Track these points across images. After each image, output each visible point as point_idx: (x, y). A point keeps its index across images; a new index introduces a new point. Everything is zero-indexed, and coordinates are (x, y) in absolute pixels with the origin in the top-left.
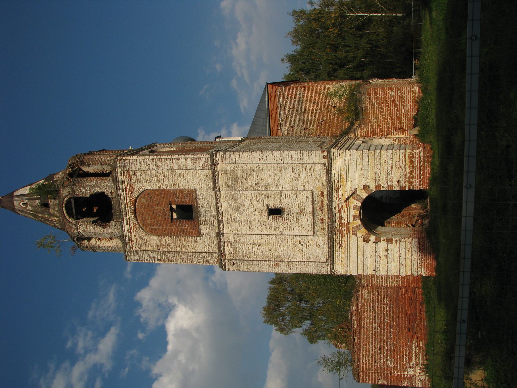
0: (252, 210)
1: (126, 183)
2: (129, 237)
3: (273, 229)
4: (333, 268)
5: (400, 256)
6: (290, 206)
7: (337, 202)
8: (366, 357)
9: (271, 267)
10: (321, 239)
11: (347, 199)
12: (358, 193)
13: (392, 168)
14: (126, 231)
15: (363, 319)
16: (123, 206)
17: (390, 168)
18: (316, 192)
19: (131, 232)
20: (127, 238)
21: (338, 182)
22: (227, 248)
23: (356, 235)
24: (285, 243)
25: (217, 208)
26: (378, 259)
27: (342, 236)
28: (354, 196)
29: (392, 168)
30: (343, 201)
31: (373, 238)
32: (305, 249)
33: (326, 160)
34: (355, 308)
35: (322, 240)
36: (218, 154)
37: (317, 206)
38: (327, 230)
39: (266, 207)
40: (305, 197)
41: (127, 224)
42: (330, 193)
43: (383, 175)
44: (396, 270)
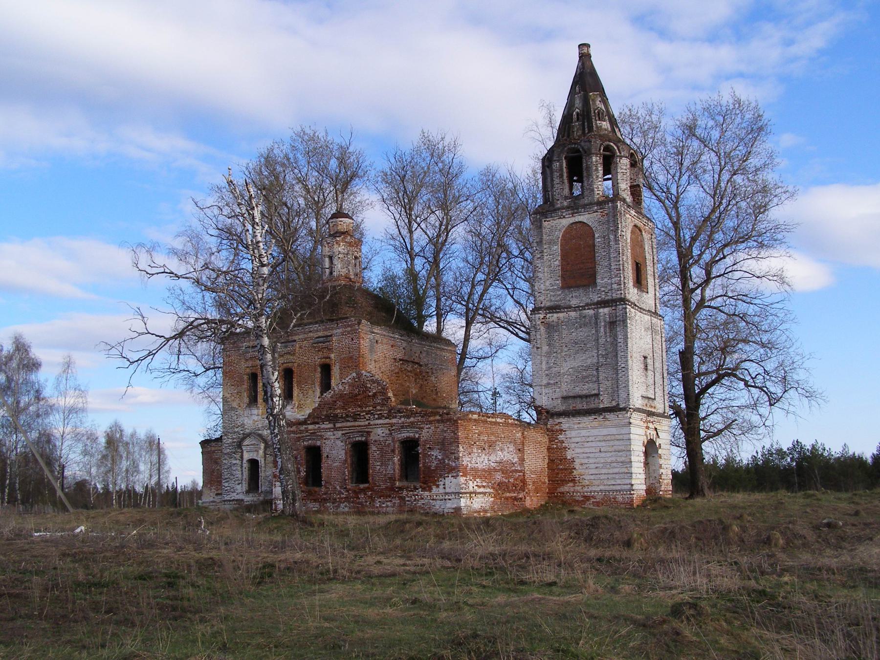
4: (634, 411)
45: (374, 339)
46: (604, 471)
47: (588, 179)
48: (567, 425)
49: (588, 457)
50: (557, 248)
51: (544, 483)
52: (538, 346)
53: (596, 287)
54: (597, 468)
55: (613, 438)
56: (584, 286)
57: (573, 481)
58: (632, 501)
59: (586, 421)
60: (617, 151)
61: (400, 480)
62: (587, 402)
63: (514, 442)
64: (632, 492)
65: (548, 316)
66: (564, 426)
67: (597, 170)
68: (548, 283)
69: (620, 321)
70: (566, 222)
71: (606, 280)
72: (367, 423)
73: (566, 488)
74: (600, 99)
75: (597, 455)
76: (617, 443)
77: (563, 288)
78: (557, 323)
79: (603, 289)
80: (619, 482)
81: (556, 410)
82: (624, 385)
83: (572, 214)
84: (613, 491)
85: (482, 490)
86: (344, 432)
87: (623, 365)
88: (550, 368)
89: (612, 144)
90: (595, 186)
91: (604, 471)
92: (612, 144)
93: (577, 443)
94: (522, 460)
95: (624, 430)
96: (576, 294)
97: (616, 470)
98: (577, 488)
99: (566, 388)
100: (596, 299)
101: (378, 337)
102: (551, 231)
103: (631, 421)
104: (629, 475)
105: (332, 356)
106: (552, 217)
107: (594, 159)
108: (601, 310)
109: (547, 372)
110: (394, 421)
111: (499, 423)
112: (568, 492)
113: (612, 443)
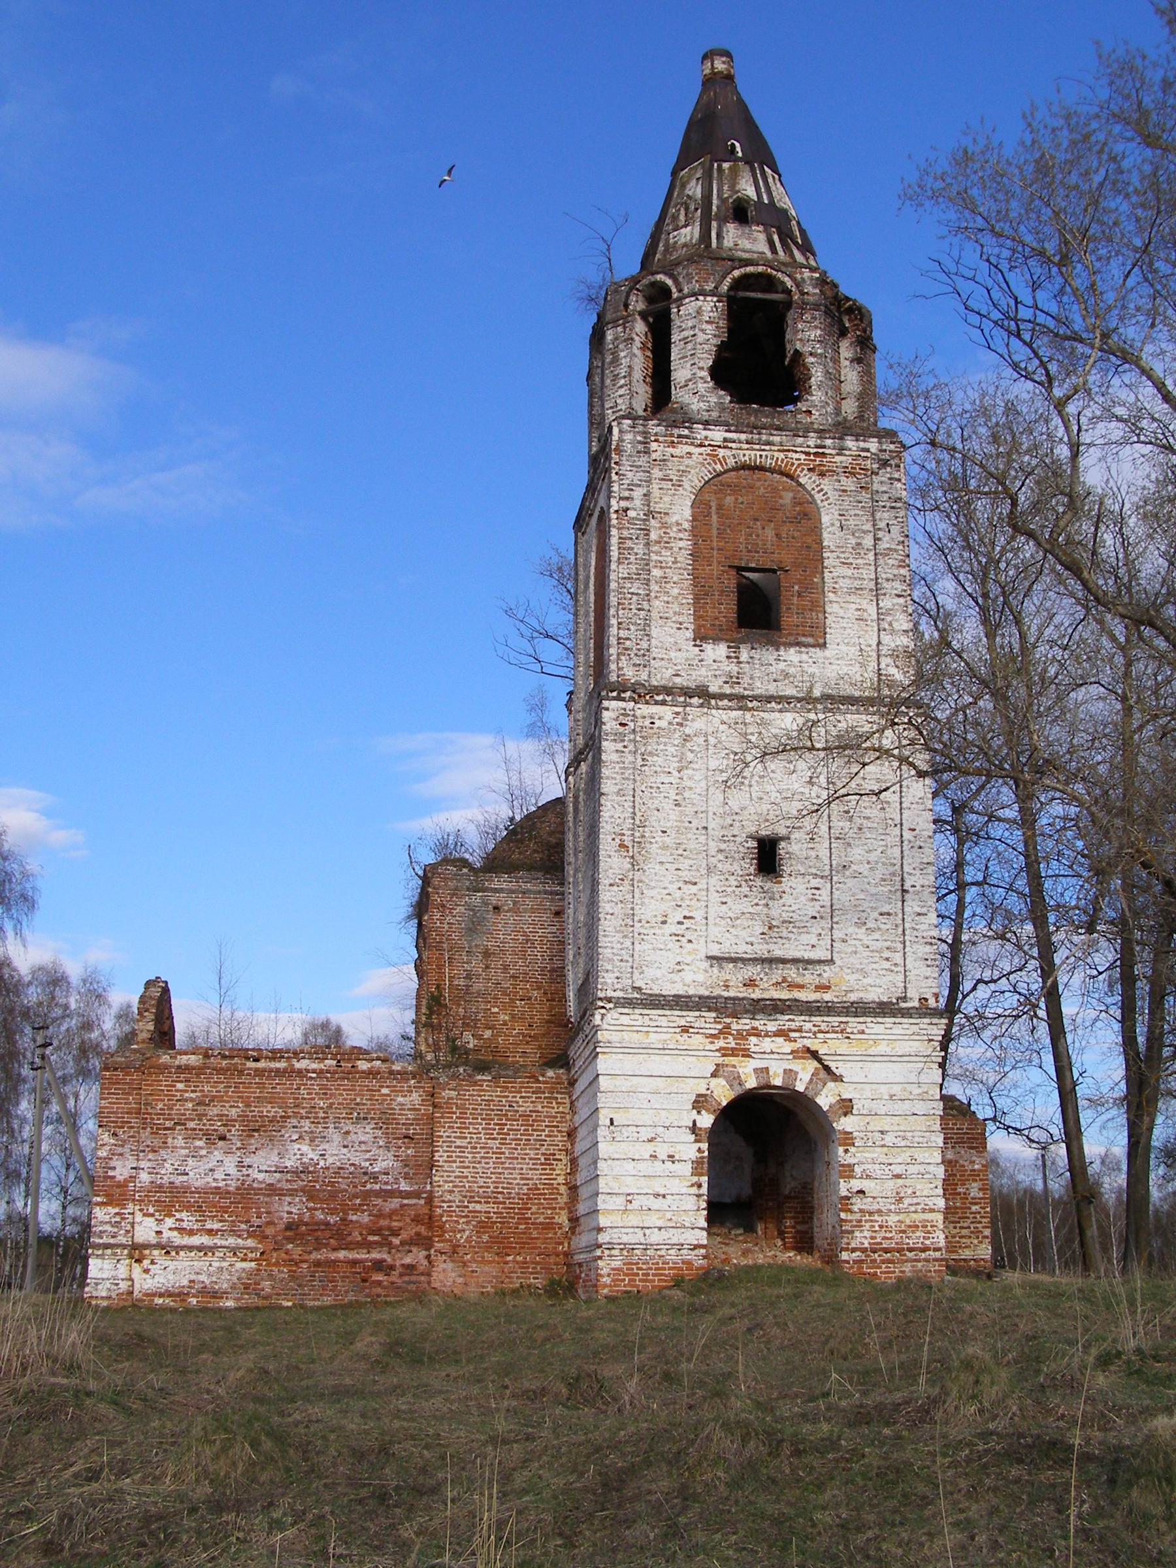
5: (657, 1195)
8: (193, 1095)
9: (617, 830)
10: (701, 977)
11: (814, 1055)
12: (831, 1085)
13: (898, 1176)
14: (705, 433)
15: (323, 1087)
16: (777, 439)
18: (828, 973)
19: (701, 445)
20: (686, 432)
21: (863, 1032)
22: (667, 712)
23: (714, 1075)
26: (646, 1134)
28: (823, 1074)
29: (898, 1176)
30: (808, 1043)
32: (668, 932)
33: (916, 1004)
37: (792, 973)
38: (726, 994)
39: (782, 831)
41: (725, 440)
42: (828, 1009)
63: (385, 1120)
85: (196, 1240)
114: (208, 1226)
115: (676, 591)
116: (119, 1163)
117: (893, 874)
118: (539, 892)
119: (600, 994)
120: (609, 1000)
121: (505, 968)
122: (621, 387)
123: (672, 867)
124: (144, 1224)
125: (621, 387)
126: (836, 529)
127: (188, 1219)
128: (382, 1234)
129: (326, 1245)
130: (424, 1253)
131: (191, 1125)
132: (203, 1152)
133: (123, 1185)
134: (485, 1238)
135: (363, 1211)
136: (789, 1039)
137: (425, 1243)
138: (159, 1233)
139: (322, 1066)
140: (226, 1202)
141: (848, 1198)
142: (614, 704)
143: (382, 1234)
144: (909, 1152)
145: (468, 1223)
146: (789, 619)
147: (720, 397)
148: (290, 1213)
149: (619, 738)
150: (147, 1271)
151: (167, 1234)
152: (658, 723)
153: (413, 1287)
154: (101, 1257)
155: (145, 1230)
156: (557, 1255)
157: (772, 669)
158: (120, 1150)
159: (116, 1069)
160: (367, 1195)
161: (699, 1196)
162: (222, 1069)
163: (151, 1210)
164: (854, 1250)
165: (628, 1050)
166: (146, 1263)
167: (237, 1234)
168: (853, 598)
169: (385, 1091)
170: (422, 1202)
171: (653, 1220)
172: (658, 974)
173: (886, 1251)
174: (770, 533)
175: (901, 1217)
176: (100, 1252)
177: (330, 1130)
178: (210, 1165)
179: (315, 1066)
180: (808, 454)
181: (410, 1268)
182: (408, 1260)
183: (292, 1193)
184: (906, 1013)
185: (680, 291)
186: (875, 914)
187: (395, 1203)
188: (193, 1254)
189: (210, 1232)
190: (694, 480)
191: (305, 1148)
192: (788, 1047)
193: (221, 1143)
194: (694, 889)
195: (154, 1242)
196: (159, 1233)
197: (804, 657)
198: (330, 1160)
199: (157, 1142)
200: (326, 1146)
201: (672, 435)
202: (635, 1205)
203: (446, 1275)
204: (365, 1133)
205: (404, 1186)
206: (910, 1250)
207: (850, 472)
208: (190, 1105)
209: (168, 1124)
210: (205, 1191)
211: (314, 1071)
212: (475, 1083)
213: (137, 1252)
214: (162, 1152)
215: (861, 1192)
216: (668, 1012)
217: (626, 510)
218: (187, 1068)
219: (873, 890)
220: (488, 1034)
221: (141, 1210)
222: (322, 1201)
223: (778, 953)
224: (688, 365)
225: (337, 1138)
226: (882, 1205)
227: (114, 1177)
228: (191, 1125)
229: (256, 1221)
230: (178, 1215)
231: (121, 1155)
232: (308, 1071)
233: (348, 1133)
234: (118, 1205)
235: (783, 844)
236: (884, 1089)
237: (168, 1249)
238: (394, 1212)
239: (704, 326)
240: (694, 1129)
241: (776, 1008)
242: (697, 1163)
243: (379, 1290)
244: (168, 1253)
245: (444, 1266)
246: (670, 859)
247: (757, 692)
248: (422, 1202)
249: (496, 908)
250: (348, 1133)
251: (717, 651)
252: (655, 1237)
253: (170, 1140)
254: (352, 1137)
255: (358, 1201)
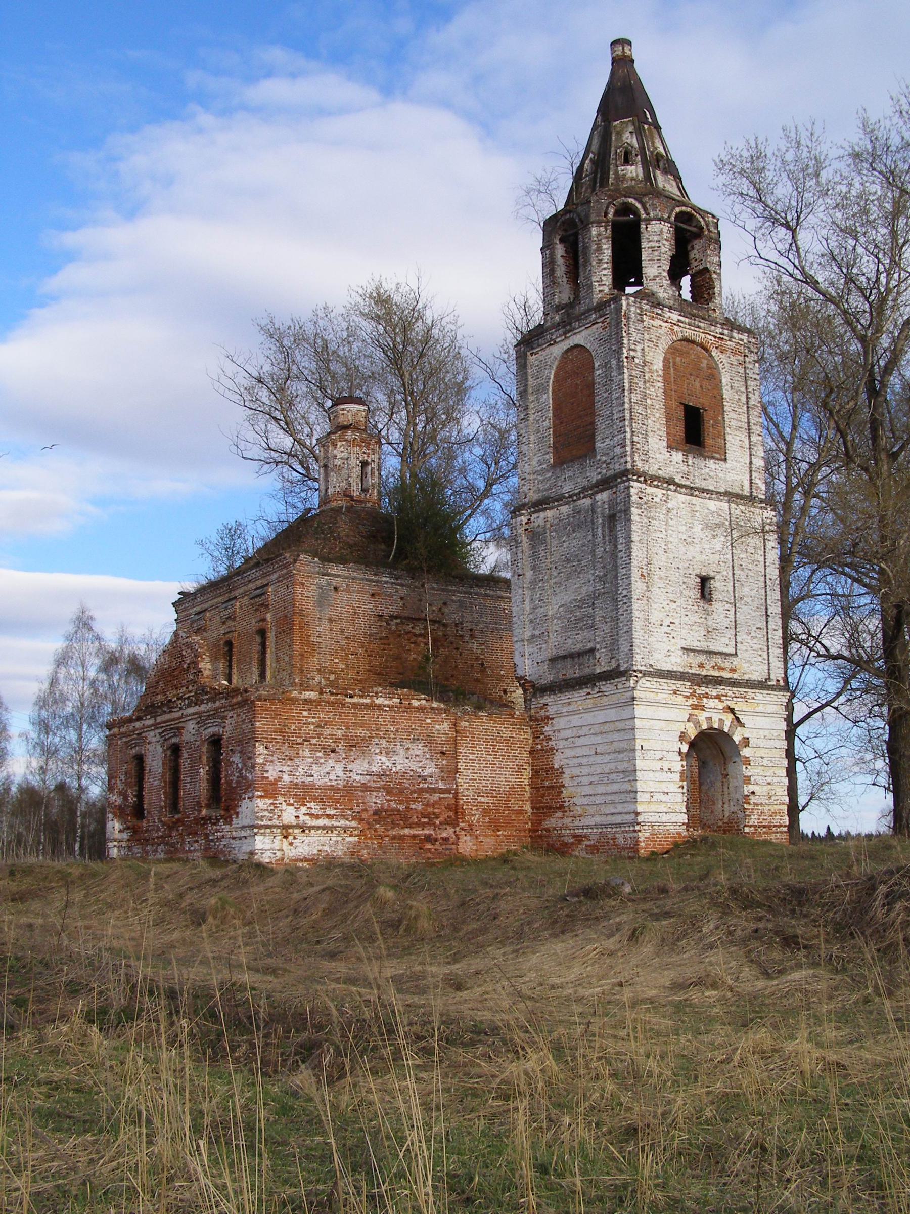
0: (707, 551)
1: (729, 343)
2: (660, 315)
3: (685, 580)
4: (644, 675)
5: (664, 793)
6: (715, 615)
7: (730, 693)
8: (314, 720)
9: (640, 565)
10: (679, 660)
11: (732, 711)
12: (739, 728)
13: (769, 784)
14: (669, 314)
15: (393, 717)
16: (702, 325)
17: (769, 780)
18: (736, 661)
19: (667, 322)
20: (660, 312)
21: (753, 698)
22: (659, 492)
23: (688, 721)
24: (671, 597)
25: (703, 491)
26: (659, 755)
27: (687, 697)
28: (735, 722)
29: (769, 784)
30: (729, 703)
31: (685, 748)
32: (663, 631)
33: (774, 683)
34: (415, 703)
35: (676, 662)
36: (773, 513)
37: (719, 660)
38: (690, 671)
39: (712, 574)
40: (727, 642)
41: (679, 321)
42: (733, 683)
43: (759, 770)
44: (644, 786)
45: (329, 584)
46: (601, 789)
47: (585, 266)
48: (555, 708)
49: (580, 765)
50: (548, 398)
51: (521, 812)
52: (520, 571)
53: (595, 456)
54: (591, 783)
55: (612, 727)
56: (580, 457)
57: (561, 807)
58: (637, 843)
59: (577, 697)
60: (642, 212)
61: (208, 806)
62: (580, 665)
63: (429, 741)
64: (637, 828)
65: (532, 519)
66: (552, 710)
67: (599, 249)
68: (534, 463)
69: (620, 512)
70: (557, 350)
71: (607, 441)
72: (180, 714)
73: (551, 822)
74: (631, 129)
75: (592, 759)
76: (616, 736)
77: (554, 467)
78: (544, 528)
79: (604, 458)
80: (620, 808)
81: (543, 682)
82: (625, 629)
83: (565, 333)
84: (612, 825)
85: (321, 822)
86: (160, 731)
87: (625, 593)
88: (535, 608)
89: (630, 200)
90: (594, 279)
91: (601, 789)
92: (630, 200)
93: (566, 739)
94: (452, 772)
95: (625, 714)
96: (571, 474)
97: (615, 787)
98: (567, 821)
99: (555, 643)
100: (594, 477)
101: (335, 582)
102: (540, 370)
103: (636, 694)
104: (632, 795)
105: (269, 616)
106: (539, 346)
107: (594, 231)
108: (599, 497)
109: (531, 616)
110: (203, 708)
111: (379, 707)
112: (555, 829)
113: (610, 737)
114: (328, 813)
115: (657, 415)
116: (271, 767)
117: (762, 605)
118: (363, 579)
119: (635, 668)
120: (641, 672)
121: (342, 631)
122: (605, 269)
123: (664, 591)
124: (288, 811)
125: (605, 269)
126: (728, 387)
127: (315, 808)
128: (429, 818)
129: (398, 825)
130: (453, 830)
131: (314, 741)
132: (322, 761)
133: (274, 783)
134: (487, 820)
135: (419, 802)
136: (721, 701)
137: (453, 823)
138: (297, 817)
139: (391, 702)
140: (337, 796)
141: (748, 796)
142: (635, 484)
143: (429, 818)
144: (773, 770)
145: (477, 810)
146: (709, 441)
147: (674, 292)
148: (376, 803)
149: (640, 507)
150: (291, 844)
151: (302, 818)
152: (656, 499)
153: (448, 852)
154: (263, 834)
155: (289, 815)
156: (525, 831)
157: (703, 472)
158: (270, 758)
159: (265, 700)
160: (422, 790)
161: (683, 793)
162: (332, 702)
163: (292, 801)
164: (751, 826)
165: (650, 703)
166: (291, 838)
167: (344, 817)
168: (738, 433)
169: (428, 721)
170: (451, 796)
171: (662, 808)
172: (660, 656)
173: (764, 827)
174: (697, 384)
175: (770, 807)
176: (262, 831)
177: (398, 747)
178: (327, 770)
179: (387, 702)
180: (715, 337)
181: (446, 839)
182: (444, 835)
183: (377, 789)
184: (771, 688)
185: (648, 214)
186: (754, 629)
187: (436, 797)
188: (319, 832)
189: (329, 816)
190: (664, 343)
191: (384, 759)
192: (721, 706)
193: (333, 755)
194: (674, 605)
195: (294, 824)
196: (297, 817)
197: (717, 466)
198: (399, 767)
199: (293, 753)
200: (395, 758)
201: (653, 312)
202: (654, 799)
203: (467, 846)
204: (418, 749)
205: (441, 785)
206: (774, 826)
207: (734, 352)
208: (312, 727)
209: (299, 740)
210: (325, 788)
211: (388, 706)
212: (479, 718)
213: (286, 830)
214: (296, 760)
215: (753, 793)
216: (669, 681)
217: (633, 358)
218: (307, 701)
219: (754, 614)
220: (332, 677)
221: (285, 801)
222: (395, 795)
223: (712, 648)
224: (656, 266)
225: (402, 752)
226: (763, 800)
227: (268, 778)
228: (314, 741)
229: (357, 809)
230: (309, 805)
231: (272, 761)
232: (385, 706)
233: (408, 749)
234: (271, 798)
235: (712, 581)
236: (762, 733)
237: (303, 828)
238: (435, 803)
239: (665, 242)
240: (680, 753)
241: (718, 681)
242: (682, 773)
243: (429, 855)
244: (303, 831)
245: (465, 838)
246: (663, 586)
247: (697, 485)
248: (451, 796)
249: (336, 589)
250: (408, 749)
251: (678, 456)
252: (665, 818)
253: (301, 752)
254: (411, 752)
255: (415, 795)
